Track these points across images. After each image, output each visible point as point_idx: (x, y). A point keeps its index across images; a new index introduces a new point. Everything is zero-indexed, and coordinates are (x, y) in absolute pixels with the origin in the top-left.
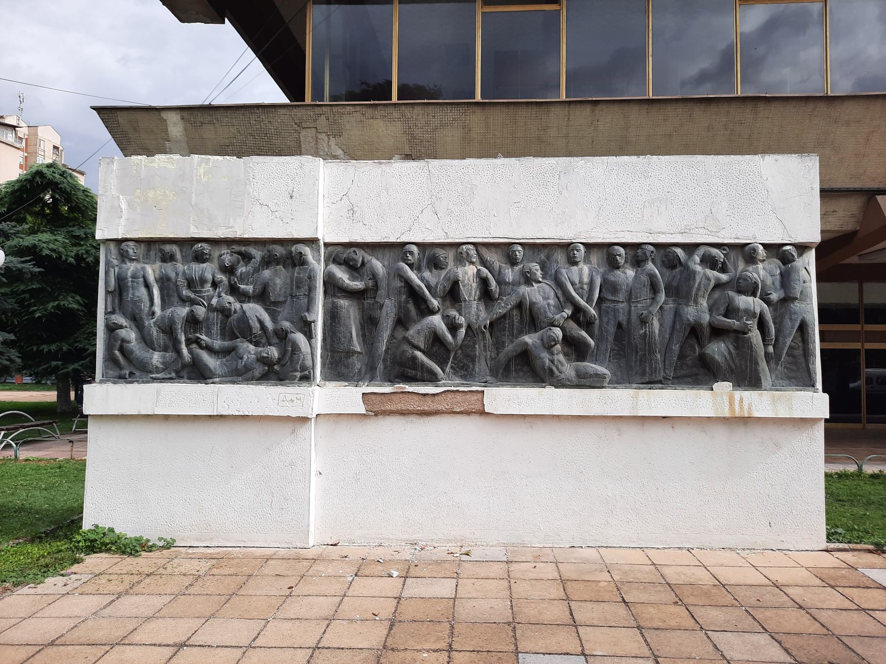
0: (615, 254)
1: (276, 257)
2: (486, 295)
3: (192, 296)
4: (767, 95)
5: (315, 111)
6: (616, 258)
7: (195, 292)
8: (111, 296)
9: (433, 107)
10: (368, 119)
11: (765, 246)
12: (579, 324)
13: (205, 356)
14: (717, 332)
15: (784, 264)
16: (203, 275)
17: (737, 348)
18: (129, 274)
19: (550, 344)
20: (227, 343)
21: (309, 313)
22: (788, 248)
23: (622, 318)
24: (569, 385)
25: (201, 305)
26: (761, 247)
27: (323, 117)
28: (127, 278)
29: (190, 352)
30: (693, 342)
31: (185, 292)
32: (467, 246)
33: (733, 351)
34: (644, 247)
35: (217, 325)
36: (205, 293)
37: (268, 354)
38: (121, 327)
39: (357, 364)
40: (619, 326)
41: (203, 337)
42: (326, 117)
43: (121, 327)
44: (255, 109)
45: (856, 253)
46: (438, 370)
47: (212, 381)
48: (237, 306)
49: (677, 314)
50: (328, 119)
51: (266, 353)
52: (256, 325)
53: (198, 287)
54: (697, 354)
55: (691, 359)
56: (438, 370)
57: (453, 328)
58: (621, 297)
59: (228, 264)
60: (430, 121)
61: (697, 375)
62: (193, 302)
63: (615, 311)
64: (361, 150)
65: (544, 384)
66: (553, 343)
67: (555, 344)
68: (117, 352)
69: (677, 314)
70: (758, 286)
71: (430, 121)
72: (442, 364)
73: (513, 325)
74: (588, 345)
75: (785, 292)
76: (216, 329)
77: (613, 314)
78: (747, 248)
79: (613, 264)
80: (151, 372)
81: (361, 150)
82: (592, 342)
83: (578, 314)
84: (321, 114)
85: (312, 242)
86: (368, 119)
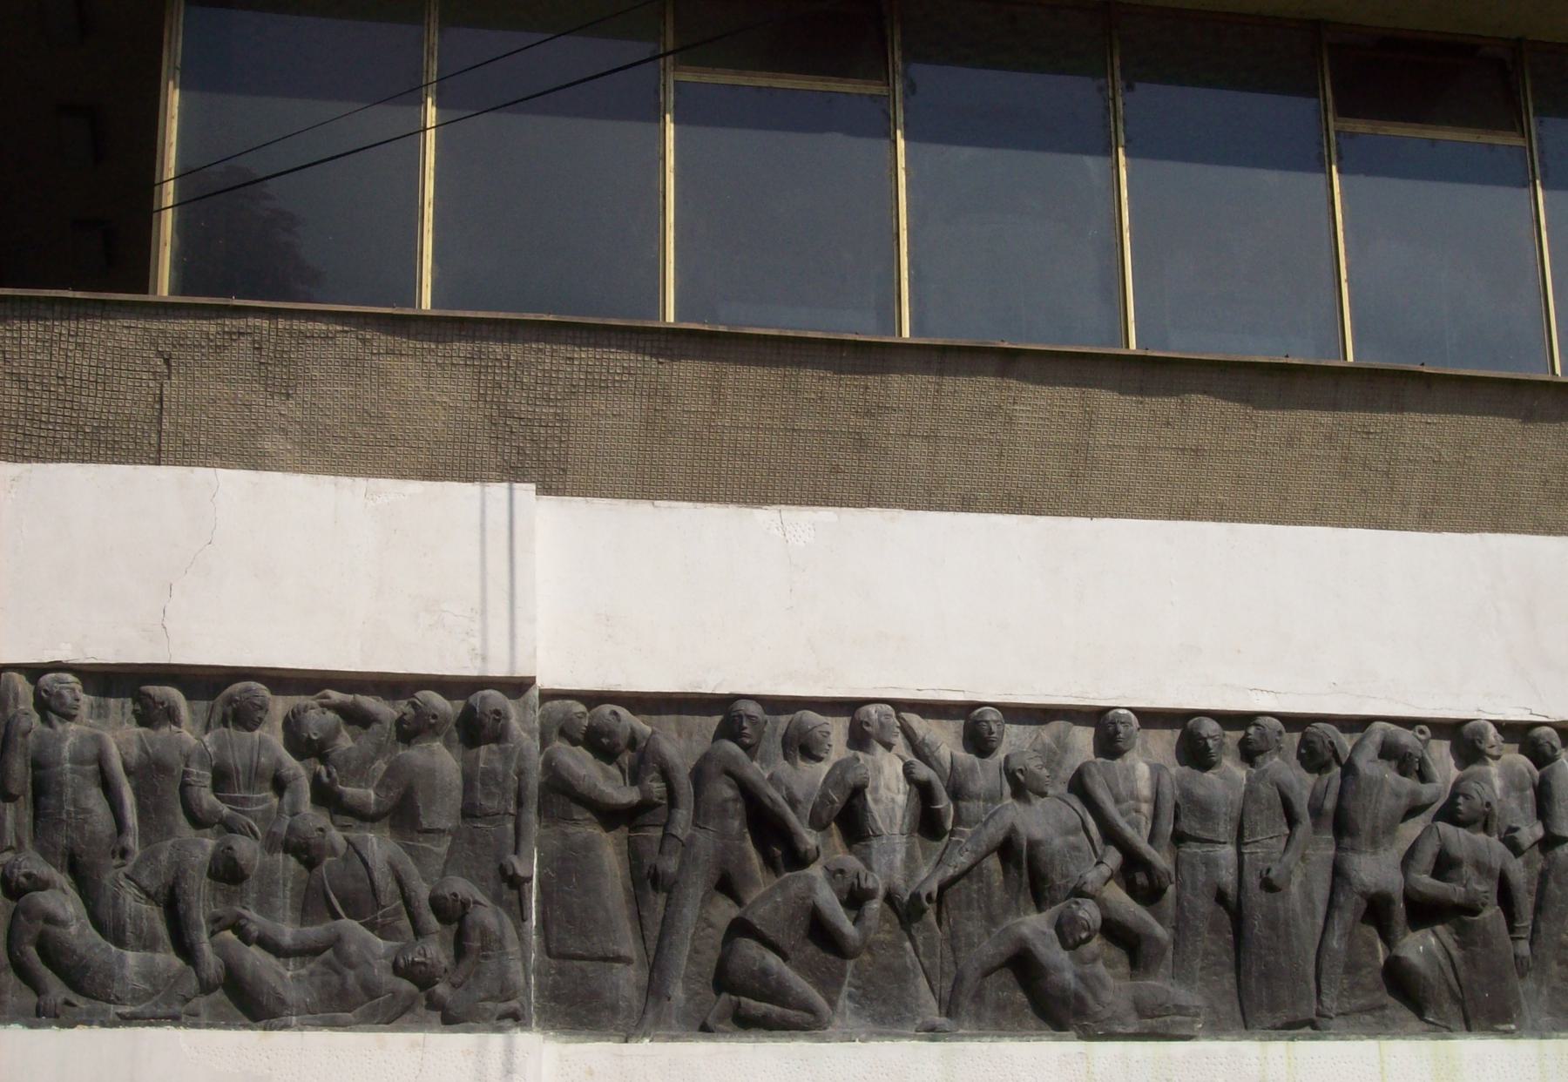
0: (1205, 736)
1: (433, 721)
2: (927, 823)
3: (225, 810)
4: (1425, 369)
5: (224, 325)
6: (1206, 744)
7: (232, 801)
8: (13, 808)
9: (570, 334)
10: (379, 354)
11: (1497, 724)
12: (1132, 890)
13: (255, 956)
14: (1424, 912)
15: (1538, 766)
16: (255, 765)
17: (1462, 945)
18: (66, 753)
19: (1078, 938)
20: (315, 932)
21: (519, 857)
22: (1121, 711)
23: (1228, 877)
24: (1120, 1034)
25: (248, 836)
26: (1492, 730)
27: (245, 343)
28: (59, 763)
29: (221, 949)
30: (1371, 932)
31: (207, 798)
32: (879, 706)
33: (1455, 953)
34: (1261, 720)
35: (285, 885)
36: (257, 805)
37: (425, 956)
38: (43, 885)
39: (627, 980)
40: (1221, 897)
41: (252, 914)
42: (254, 341)
43: (43, 885)
44: (42, 306)
45: (408, 698)
46: (819, 1000)
47: (283, 1023)
48: (337, 837)
49: (1339, 873)
50: (260, 349)
51: (420, 954)
52: (386, 883)
53: (239, 790)
54: (1382, 961)
55: (1370, 973)
56: (819, 1000)
57: (855, 899)
58: (1225, 829)
59: (315, 734)
60: (558, 371)
61: (1383, 1007)
62: (228, 826)
63: (1210, 863)
64: (344, 439)
65: (1002, 1032)
66: (1084, 935)
67: (1088, 939)
68: (32, 951)
69: (1339, 873)
70: (540, 812)
71: (558, 371)
72: (829, 984)
73: (989, 896)
74: (1153, 939)
75: (1546, 827)
76: (284, 900)
77: (1204, 869)
78: (1468, 726)
79: (1195, 753)
80: (119, 1001)
81: (344, 439)
82: (1161, 932)
83: (1133, 870)
84: (242, 334)
85: (517, 687)
86: (379, 354)
